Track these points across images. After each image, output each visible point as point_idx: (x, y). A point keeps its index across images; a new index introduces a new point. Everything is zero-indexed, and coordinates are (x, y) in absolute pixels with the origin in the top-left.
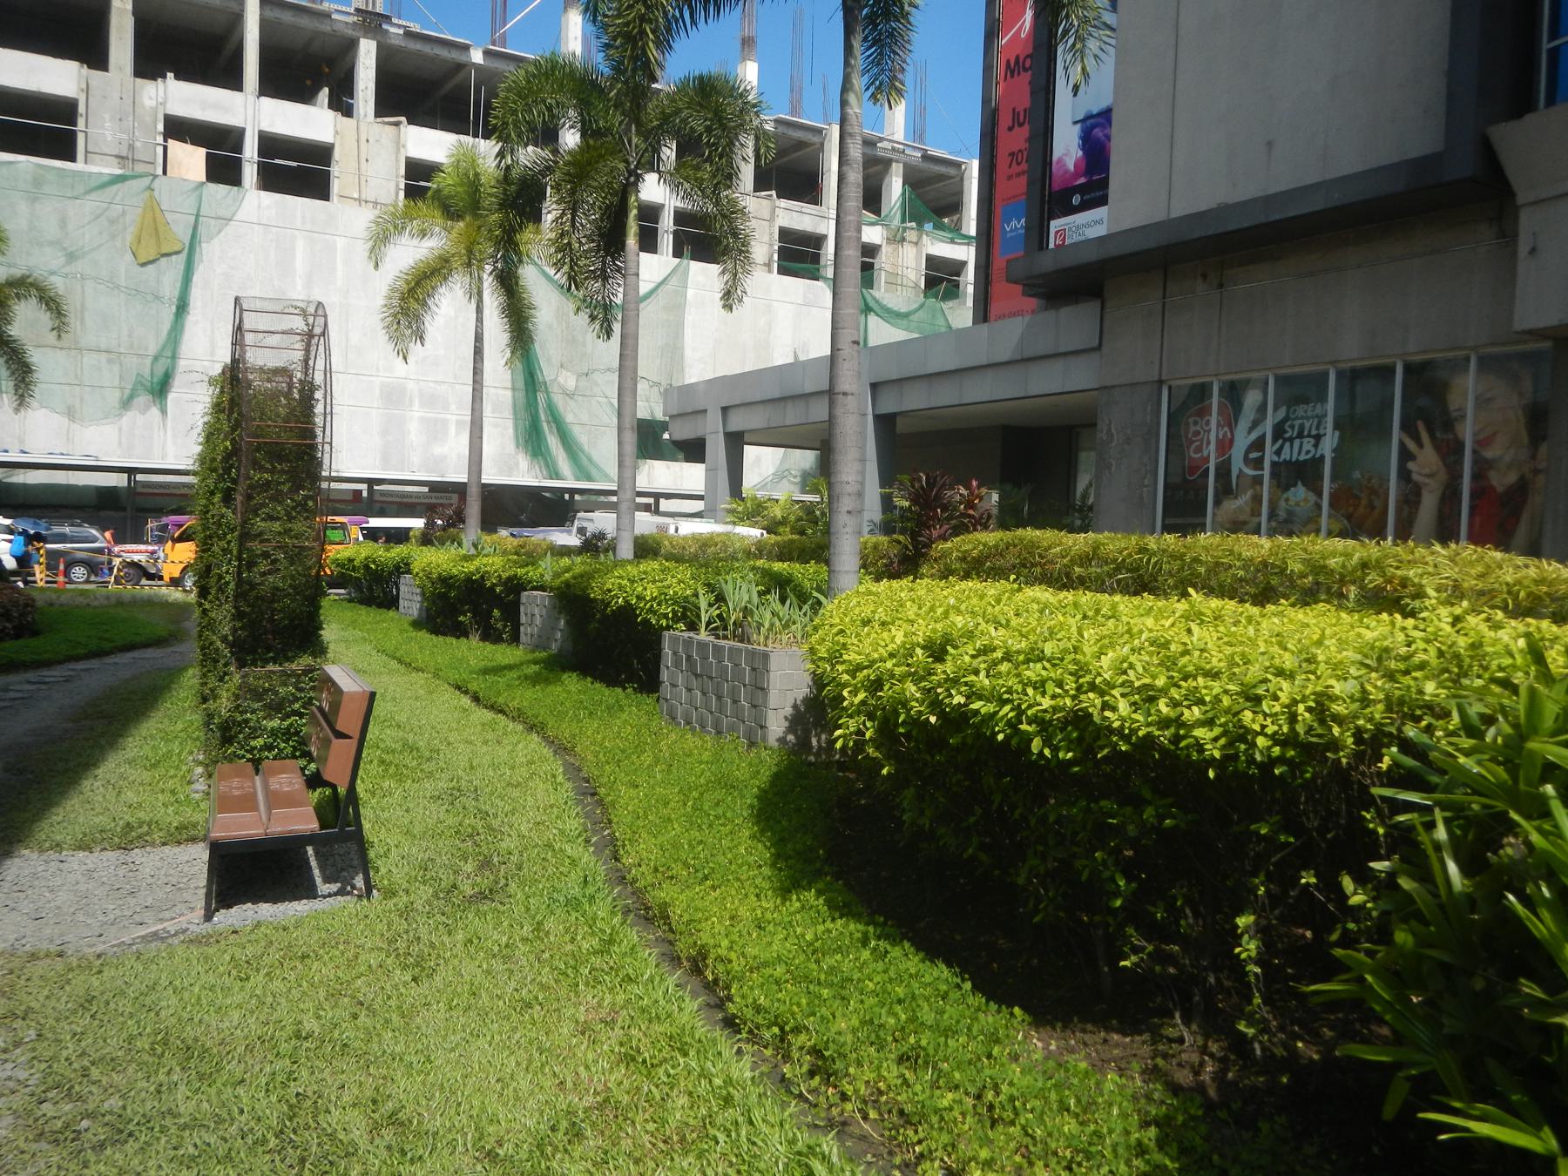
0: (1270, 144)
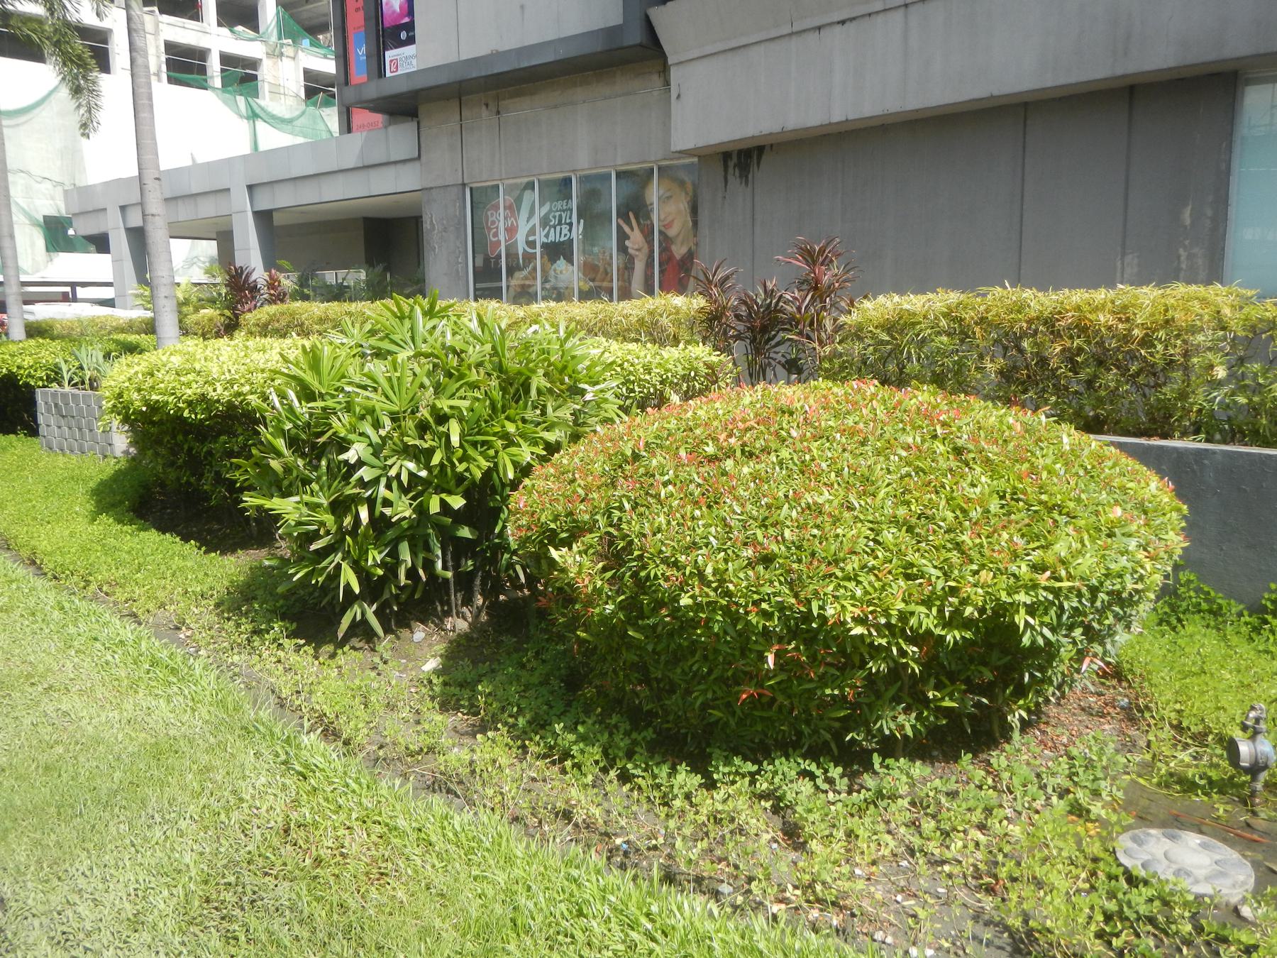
0: (522, 7)
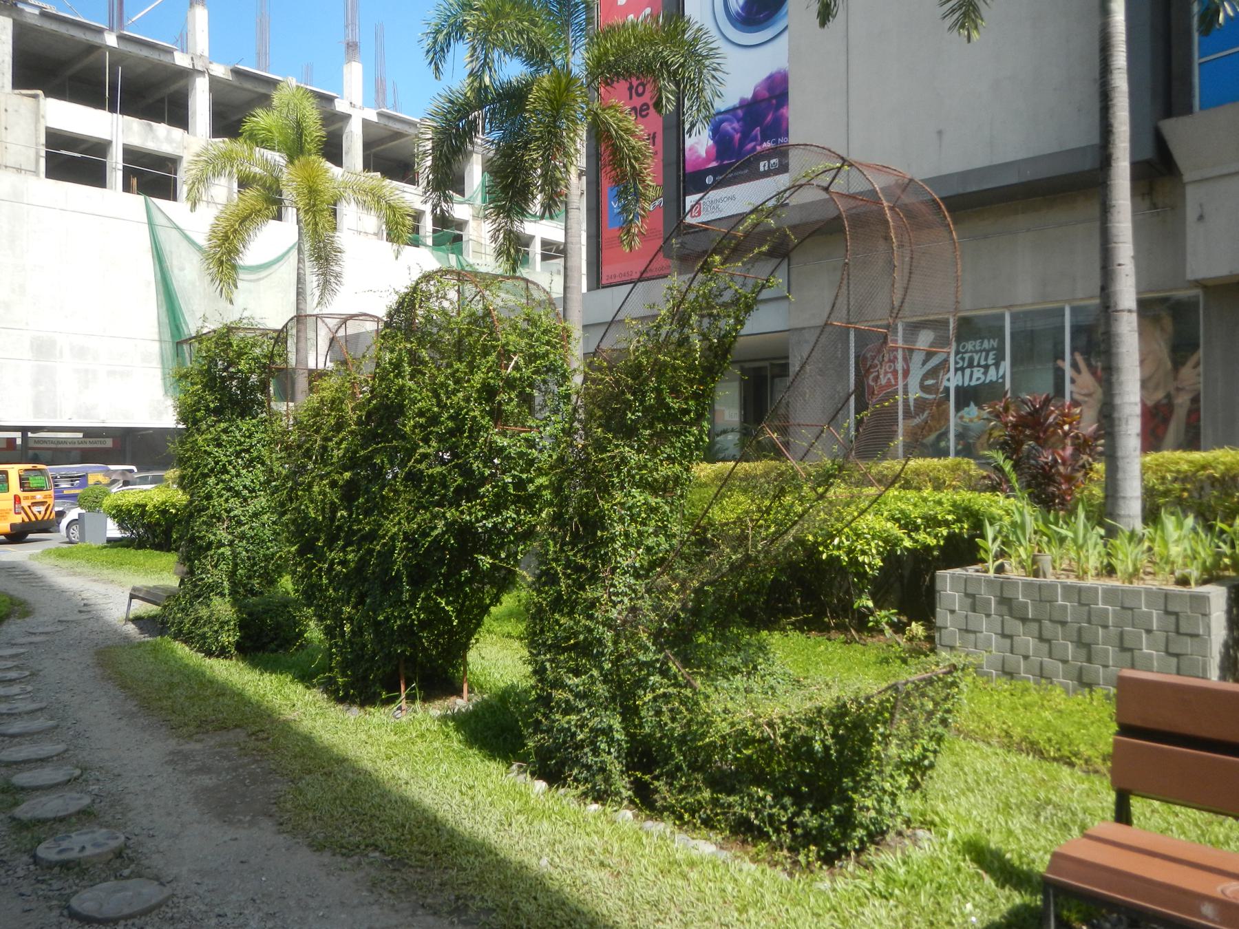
0: (940, 133)
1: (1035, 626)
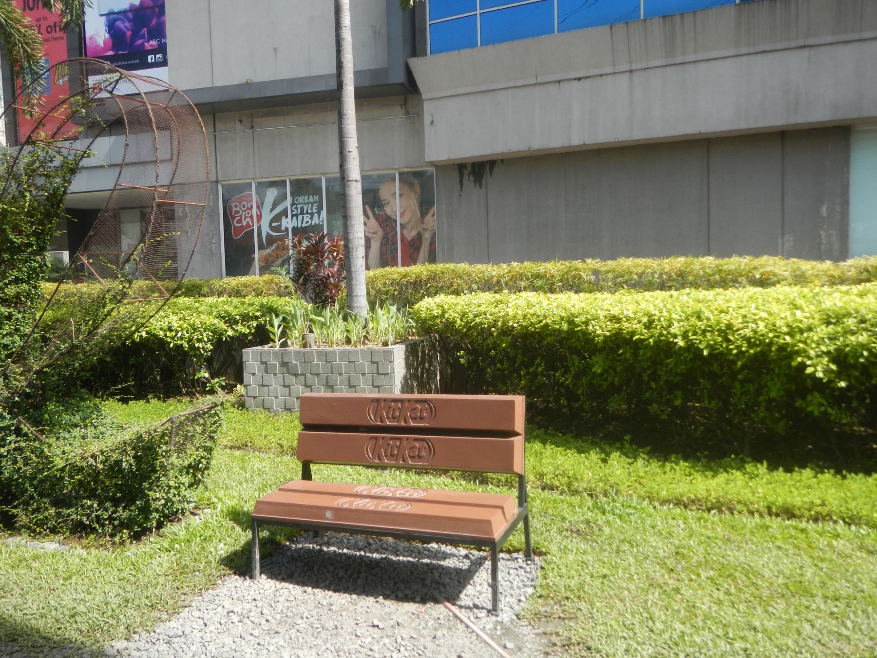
0: (275, 49)
1: (302, 378)
